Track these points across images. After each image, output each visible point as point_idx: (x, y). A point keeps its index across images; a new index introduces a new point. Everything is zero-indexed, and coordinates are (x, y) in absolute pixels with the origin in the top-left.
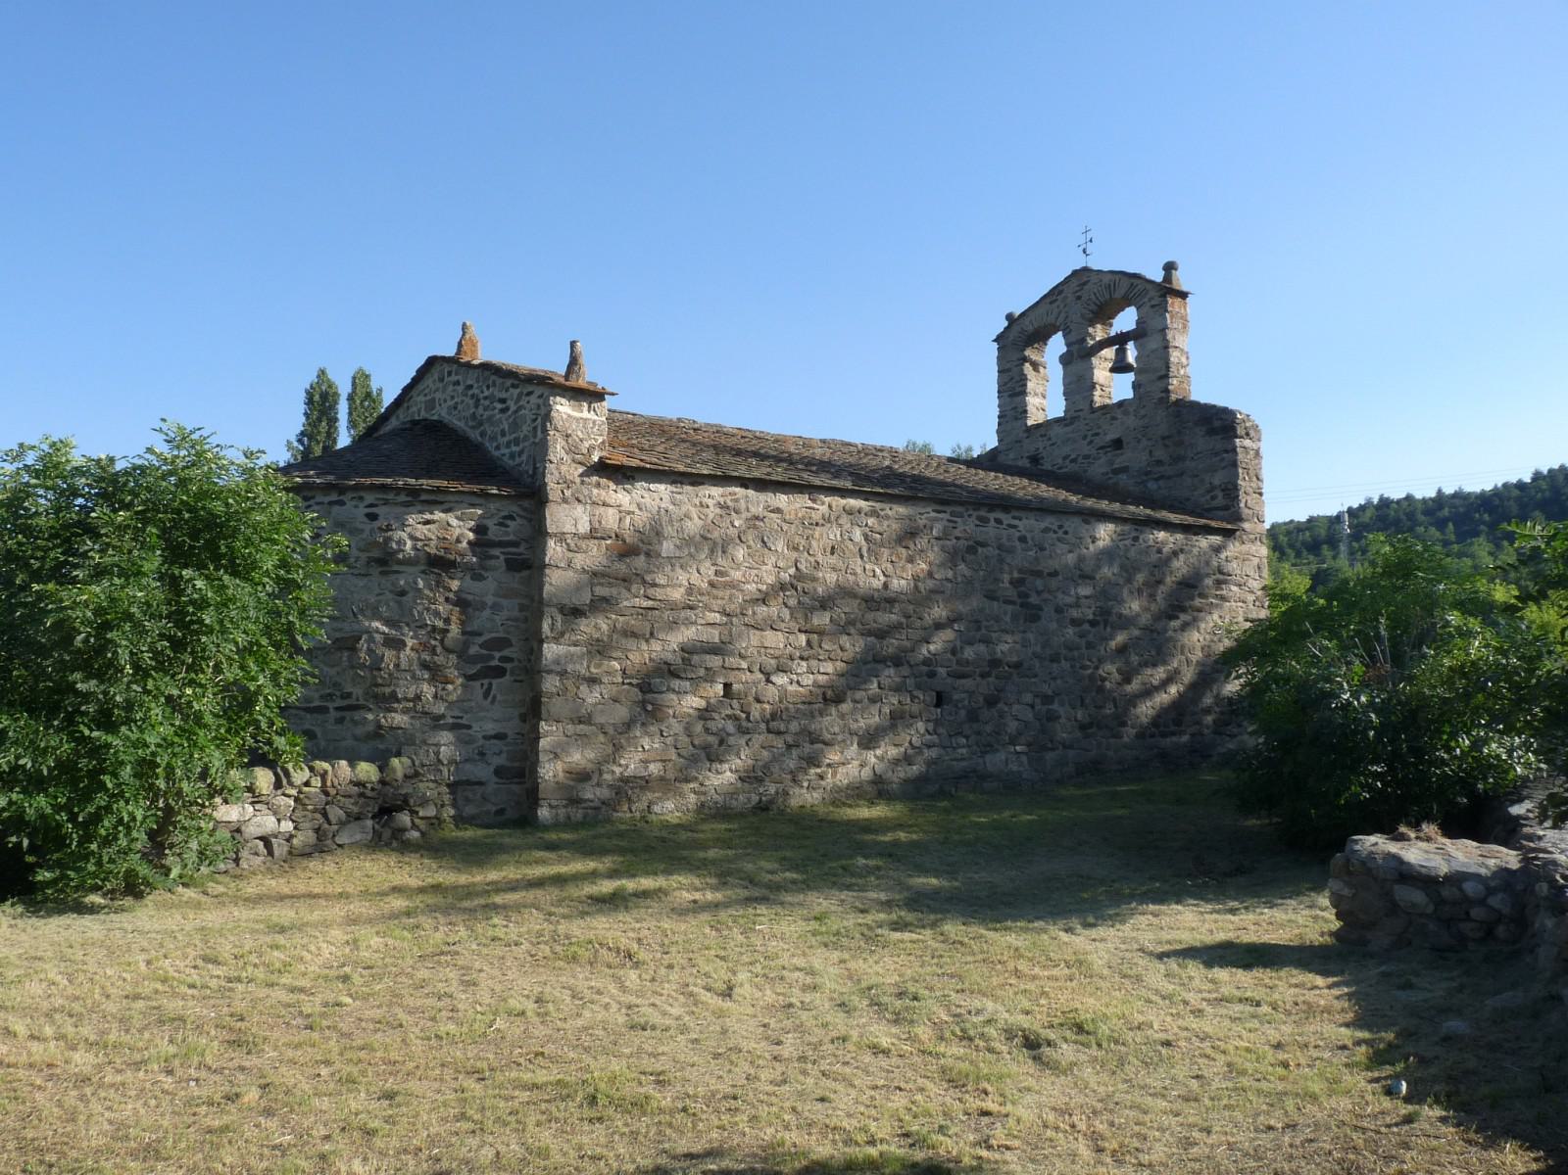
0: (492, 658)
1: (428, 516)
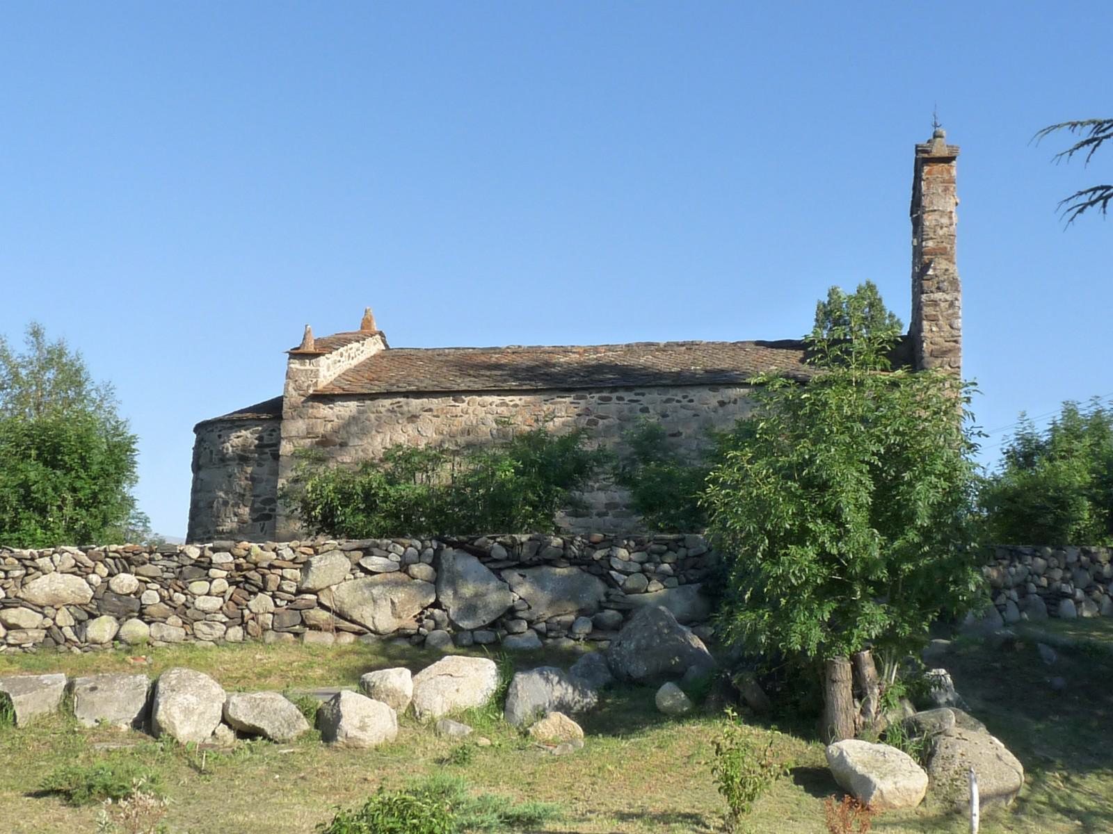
0: (265, 509)
1: (239, 434)
